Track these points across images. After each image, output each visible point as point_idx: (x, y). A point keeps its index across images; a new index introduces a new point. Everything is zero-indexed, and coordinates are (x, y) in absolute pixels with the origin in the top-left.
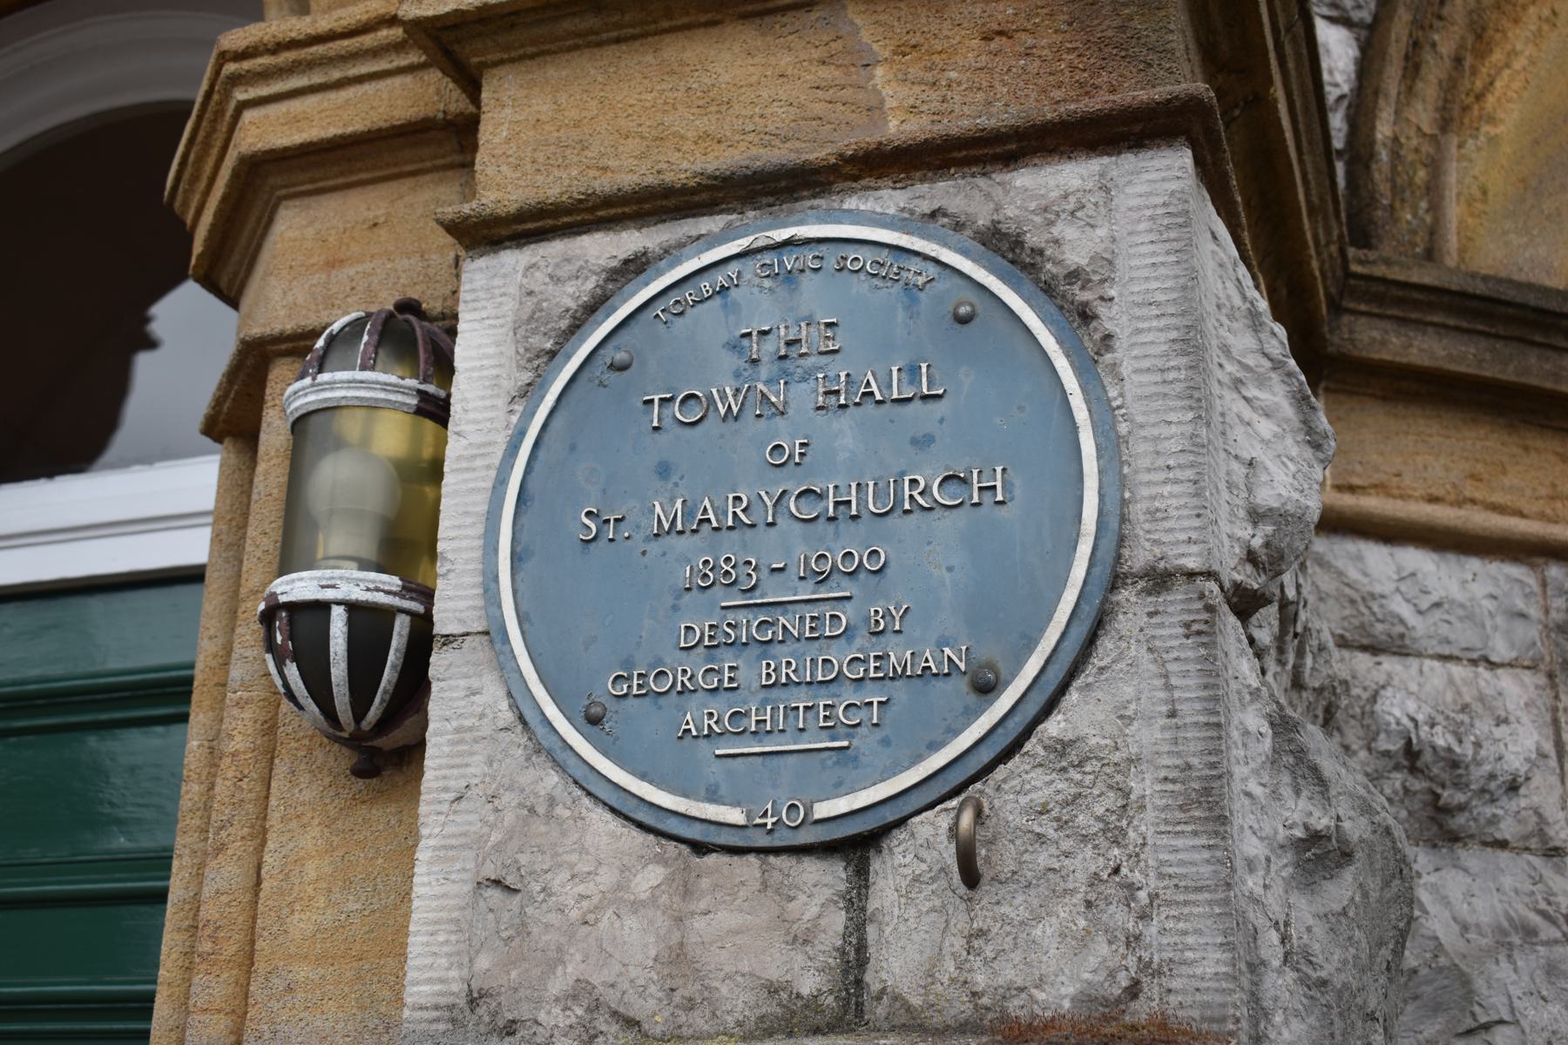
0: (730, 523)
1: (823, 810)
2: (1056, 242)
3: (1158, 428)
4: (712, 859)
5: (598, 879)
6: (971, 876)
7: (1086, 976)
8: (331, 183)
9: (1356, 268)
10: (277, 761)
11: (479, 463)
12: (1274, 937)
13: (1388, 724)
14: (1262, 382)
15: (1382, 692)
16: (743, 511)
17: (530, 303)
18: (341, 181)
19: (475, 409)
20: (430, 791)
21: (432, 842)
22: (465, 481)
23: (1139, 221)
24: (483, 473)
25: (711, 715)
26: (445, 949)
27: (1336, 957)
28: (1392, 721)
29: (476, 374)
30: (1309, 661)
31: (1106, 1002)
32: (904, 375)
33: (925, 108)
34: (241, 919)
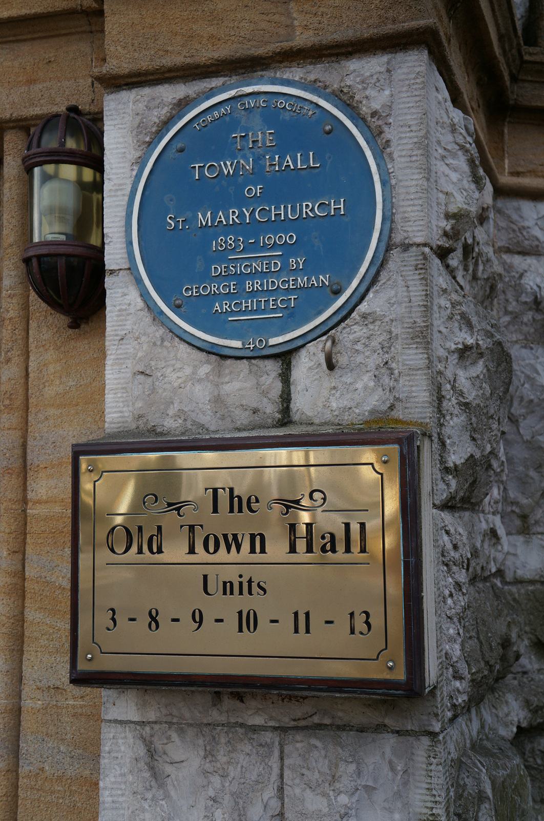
0: (231, 223)
1: (273, 341)
2: (367, 97)
3: (408, 179)
4: (229, 362)
5: (184, 370)
6: (331, 366)
7: (374, 403)
8: (25, 37)
9: (527, 58)
10: (31, 322)
11: (119, 193)
12: (448, 387)
13: (526, 289)
14: (454, 155)
15: (525, 274)
16: (236, 217)
17: (138, 119)
18: (29, 36)
19: (116, 168)
20: (110, 336)
21: (112, 357)
22: (114, 201)
23: (403, 86)
24: (121, 198)
25: (226, 304)
26: (121, 399)
27: (473, 394)
28: (529, 287)
29: (114, 151)
30: (481, 268)
31: (382, 412)
32: (302, 158)
33: (311, 26)
34: (20, 391)
